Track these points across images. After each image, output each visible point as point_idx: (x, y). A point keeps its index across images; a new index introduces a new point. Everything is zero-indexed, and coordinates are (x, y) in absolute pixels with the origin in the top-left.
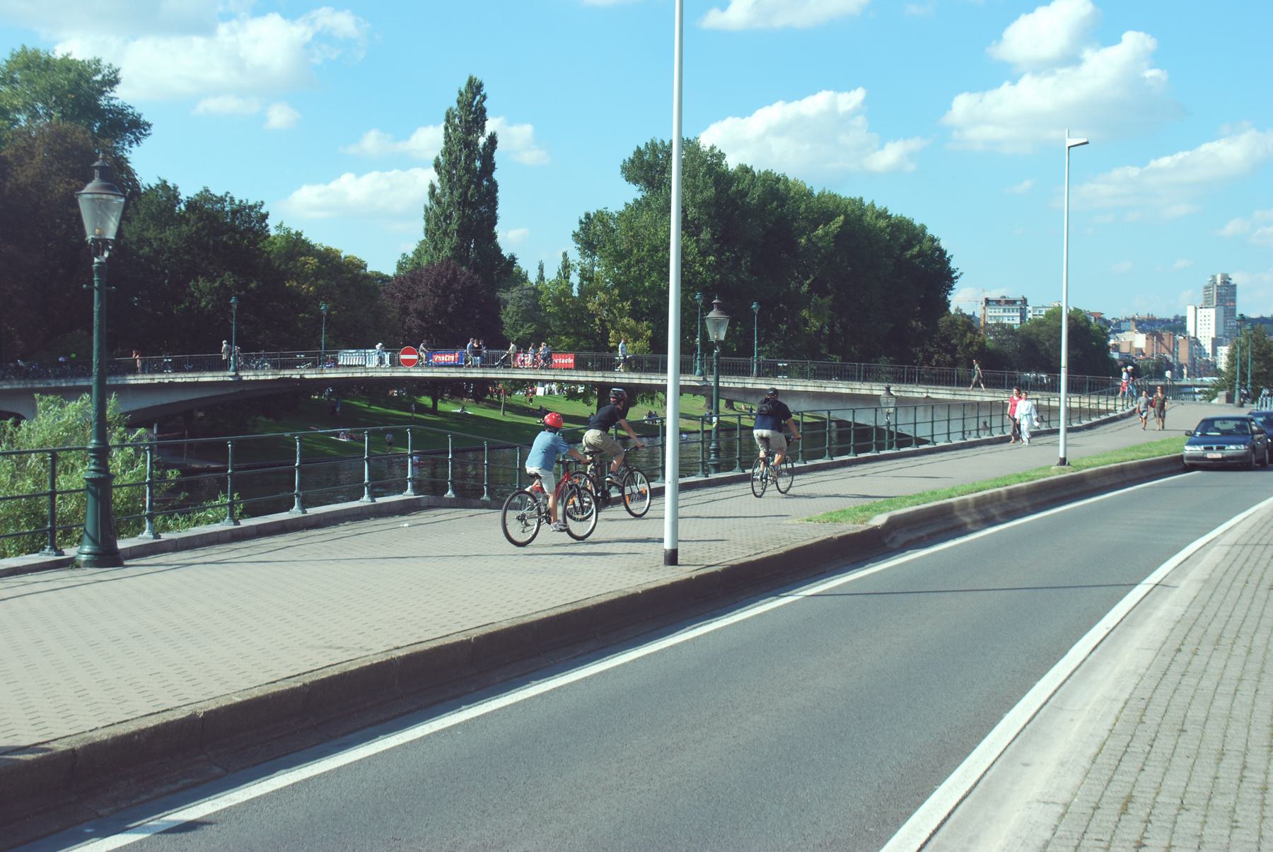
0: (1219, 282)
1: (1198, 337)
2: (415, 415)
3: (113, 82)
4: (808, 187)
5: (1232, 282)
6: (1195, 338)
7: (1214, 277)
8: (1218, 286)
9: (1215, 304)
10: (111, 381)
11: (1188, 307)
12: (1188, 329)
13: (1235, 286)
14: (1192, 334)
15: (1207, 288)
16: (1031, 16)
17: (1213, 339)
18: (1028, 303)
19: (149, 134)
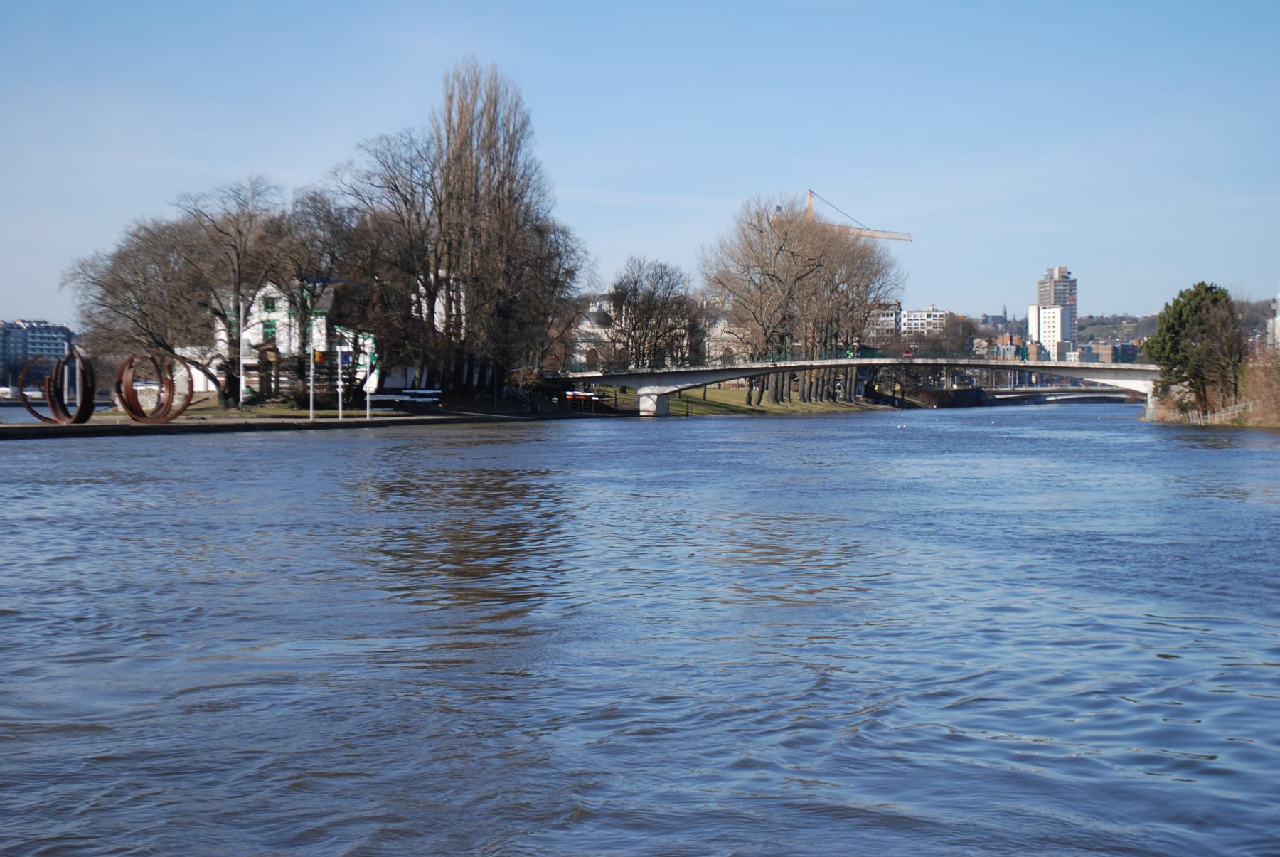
0: (1056, 277)
1: (1042, 341)
2: (770, 365)
3: (1166, 305)
4: (546, 188)
5: (1072, 277)
6: (1038, 342)
7: (1051, 270)
8: (1055, 282)
9: (1052, 302)
10: (417, 386)
11: (1030, 307)
12: (1030, 333)
13: (1075, 281)
14: (1035, 338)
15: (1042, 284)
16: (1146, 315)
17: (1059, 344)
18: (902, 307)
19: (907, 276)
